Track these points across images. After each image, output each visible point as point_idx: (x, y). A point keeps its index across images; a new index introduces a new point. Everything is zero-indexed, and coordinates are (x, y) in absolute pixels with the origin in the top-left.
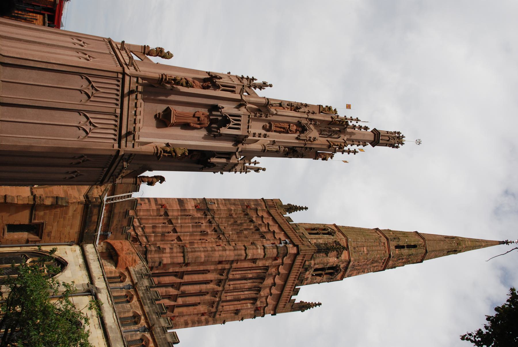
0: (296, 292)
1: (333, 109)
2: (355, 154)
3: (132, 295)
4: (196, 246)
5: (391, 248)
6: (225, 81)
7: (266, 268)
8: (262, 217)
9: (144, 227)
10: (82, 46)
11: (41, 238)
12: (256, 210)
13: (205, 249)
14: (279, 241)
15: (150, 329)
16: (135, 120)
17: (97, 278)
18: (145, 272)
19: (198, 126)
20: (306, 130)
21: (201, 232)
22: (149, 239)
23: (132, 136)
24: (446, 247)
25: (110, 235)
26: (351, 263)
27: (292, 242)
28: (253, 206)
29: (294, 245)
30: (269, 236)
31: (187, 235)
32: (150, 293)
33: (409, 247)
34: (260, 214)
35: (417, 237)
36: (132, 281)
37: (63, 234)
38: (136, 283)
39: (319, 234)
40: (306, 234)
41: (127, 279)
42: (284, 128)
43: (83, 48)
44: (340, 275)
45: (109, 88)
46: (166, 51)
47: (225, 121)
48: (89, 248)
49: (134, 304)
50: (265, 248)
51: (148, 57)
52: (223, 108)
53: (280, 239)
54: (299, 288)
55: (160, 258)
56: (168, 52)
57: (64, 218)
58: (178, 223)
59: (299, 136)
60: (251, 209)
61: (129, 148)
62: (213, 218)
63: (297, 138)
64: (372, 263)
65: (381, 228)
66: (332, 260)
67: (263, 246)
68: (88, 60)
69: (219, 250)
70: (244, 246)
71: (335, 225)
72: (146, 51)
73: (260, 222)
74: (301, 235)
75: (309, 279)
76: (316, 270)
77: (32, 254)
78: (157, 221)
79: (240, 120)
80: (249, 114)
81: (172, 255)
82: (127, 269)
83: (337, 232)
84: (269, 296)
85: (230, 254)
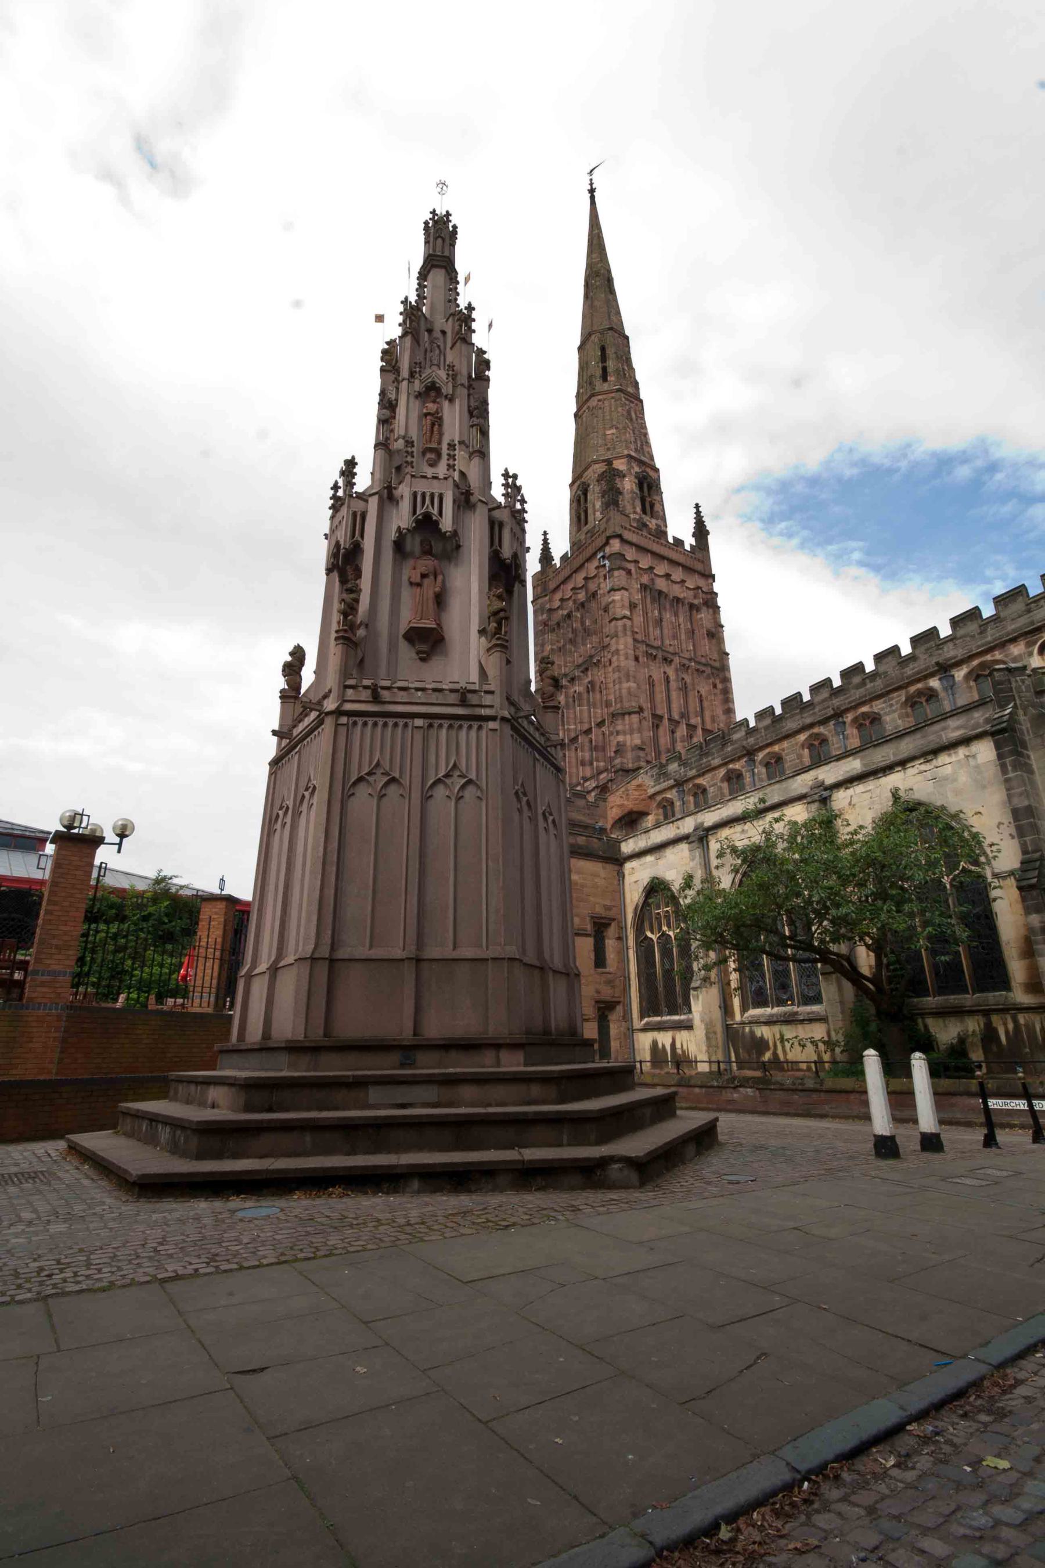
0: (679, 542)
1: (386, 347)
2: (474, 309)
4: (612, 697)
5: (605, 389)
6: (342, 536)
7: (644, 587)
8: (562, 600)
9: (583, 778)
11: (614, 920)
12: (550, 610)
14: (601, 569)
15: (750, 754)
17: (678, 831)
18: (656, 770)
19: (440, 578)
20: (433, 383)
22: (602, 768)
25: (600, 824)
26: (633, 454)
27: (601, 548)
28: (545, 616)
29: (607, 543)
30: (592, 586)
31: (595, 713)
33: (604, 358)
34: (557, 604)
35: (587, 346)
36: (671, 788)
38: (675, 780)
40: (585, 529)
41: (668, 796)
42: (433, 425)
43: (291, 807)
44: (651, 473)
46: (289, 659)
47: (426, 524)
48: (628, 847)
51: (302, 691)
52: (399, 528)
53: (597, 568)
55: (633, 750)
57: (583, 886)
58: (576, 729)
59: (446, 397)
61: (496, 700)
62: (566, 675)
63: (451, 400)
64: (631, 420)
66: (628, 485)
69: (618, 660)
70: (610, 622)
71: (571, 486)
72: (290, 695)
73: (571, 603)
75: (659, 522)
76: (644, 511)
77: (639, 929)
78: (574, 760)
80: (408, 477)
82: (652, 797)
85: (624, 644)
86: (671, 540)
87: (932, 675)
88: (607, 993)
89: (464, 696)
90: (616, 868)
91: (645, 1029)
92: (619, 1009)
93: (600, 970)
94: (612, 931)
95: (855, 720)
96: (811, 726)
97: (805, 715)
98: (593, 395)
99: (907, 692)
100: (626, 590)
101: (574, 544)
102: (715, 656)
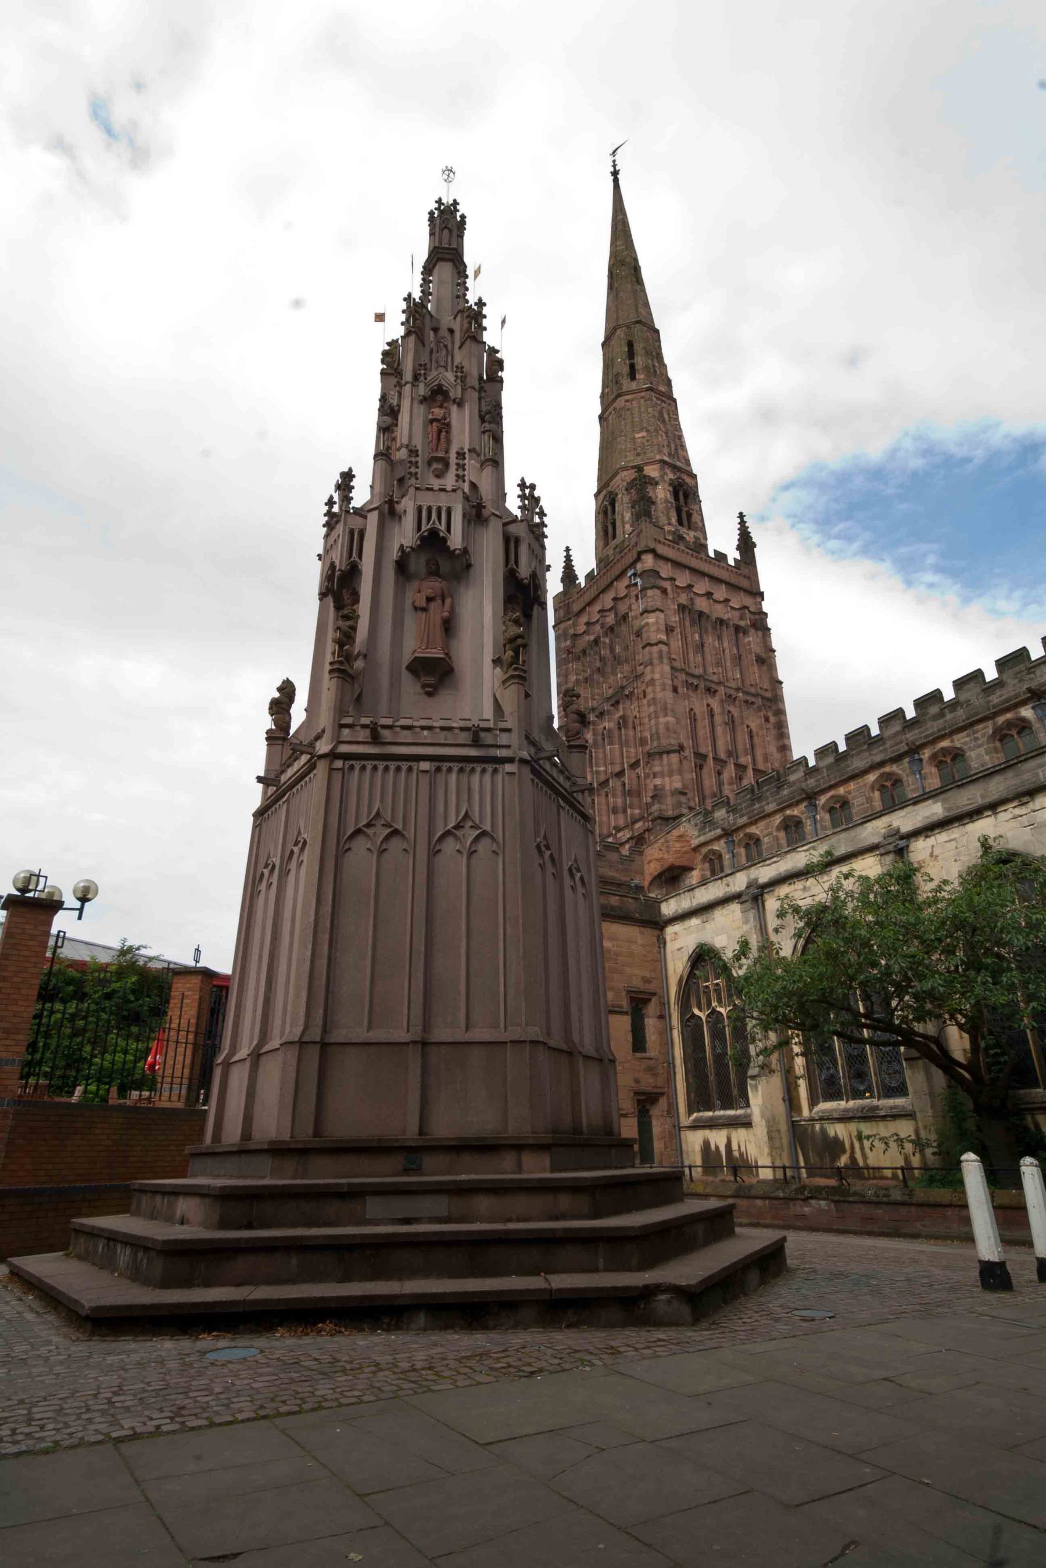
0: (721, 557)
1: (387, 348)
2: (485, 304)
3: (746, 835)
10: (274, 866)
11: (654, 994)
12: (575, 635)
13: (653, 716)
14: (632, 589)
15: (810, 797)
16: (443, 728)
17: (728, 889)
18: (700, 818)
19: (448, 601)
20: (440, 386)
21: (620, 728)
23: (482, 734)
24: (629, 286)
25: (636, 881)
26: (666, 459)
27: (633, 565)
28: (568, 643)
29: (638, 559)
30: (623, 608)
32: (739, 804)
33: (631, 354)
35: (613, 342)
36: (718, 838)
37: (645, 956)
38: (723, 829)
39: (615, 520)
40: (613, 543)
42: (440, 432)
44: (688, 480)
45: (372, 791)
46: (277, 695)
47: (433, 541)
49: (762, 831)
50: (646, 611)
51: (292, 731)
52: (402, 546)
53: (628, 587)
54: (715, 551)
56: (279, 689)
57: (617, 955)
60: (573, 646)
61: (514, 739)
62: (593, 709)
64: (664, 421)
65: (599, 411)
66: (661, 493)
67: (642, 614)
68: (305, 842)
69: (654, 692)
70: (644, 648)
71: (596, 496)
72: (278, 736)
73: (598, 627)
74: (618, 550)
75: (699, 534)
76: (680, 522)
78: (604, 807)
79: (429, 509)
81: (666, 773)
82: (696, 849)
83: (610, 489)
84: (731, 604)
85: (660, 673)
86: (712, 554)
87: (1023, 703)
88: (648, 1083)
89: (476, 735)
90: (657, 932)
91: (695, 1127)
92: (663, 1102)
93: (638, 1055)
94: (652, 1009)
95: (934, 757)
96: (882, 764)
97: (875, 751)
98: (619, 396)
99: (994, 724)
100: (662, 611)
101: (601, 561)
102: (766, 685)
